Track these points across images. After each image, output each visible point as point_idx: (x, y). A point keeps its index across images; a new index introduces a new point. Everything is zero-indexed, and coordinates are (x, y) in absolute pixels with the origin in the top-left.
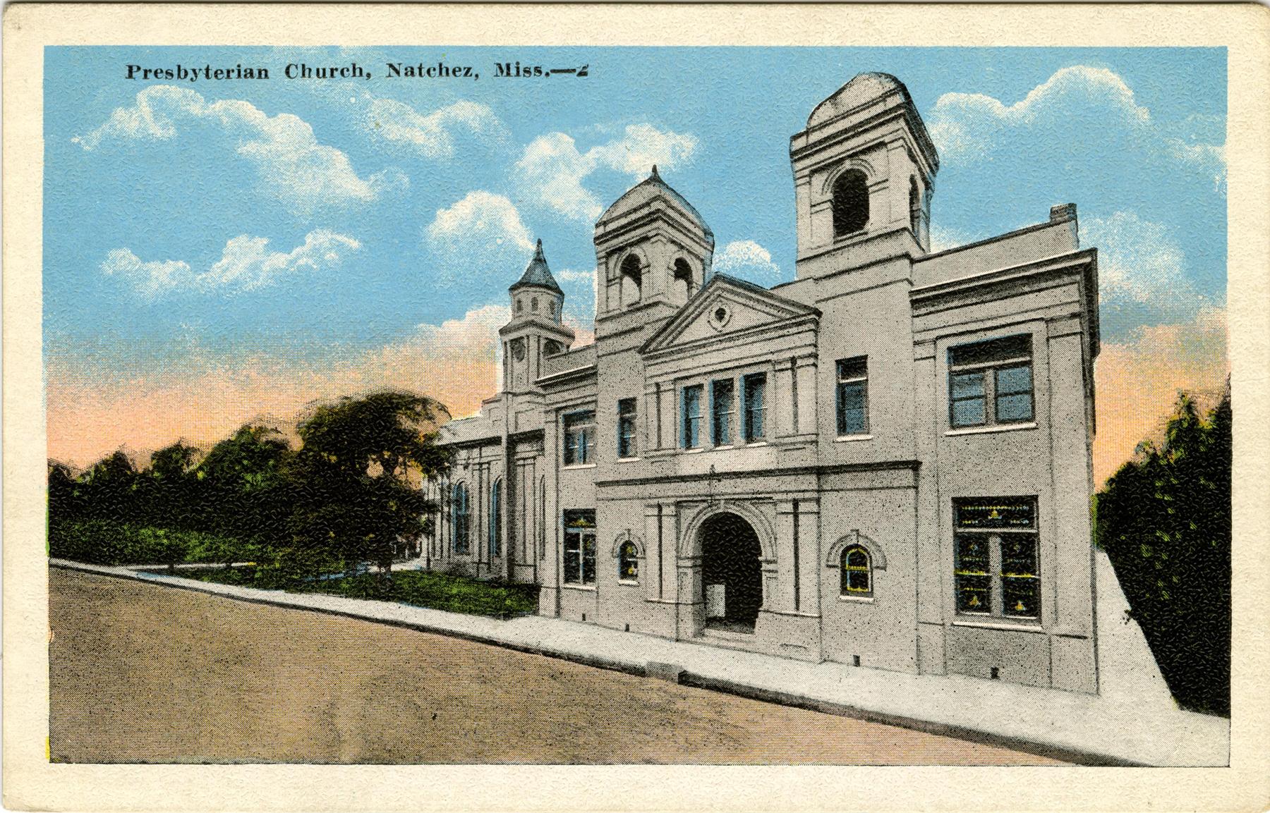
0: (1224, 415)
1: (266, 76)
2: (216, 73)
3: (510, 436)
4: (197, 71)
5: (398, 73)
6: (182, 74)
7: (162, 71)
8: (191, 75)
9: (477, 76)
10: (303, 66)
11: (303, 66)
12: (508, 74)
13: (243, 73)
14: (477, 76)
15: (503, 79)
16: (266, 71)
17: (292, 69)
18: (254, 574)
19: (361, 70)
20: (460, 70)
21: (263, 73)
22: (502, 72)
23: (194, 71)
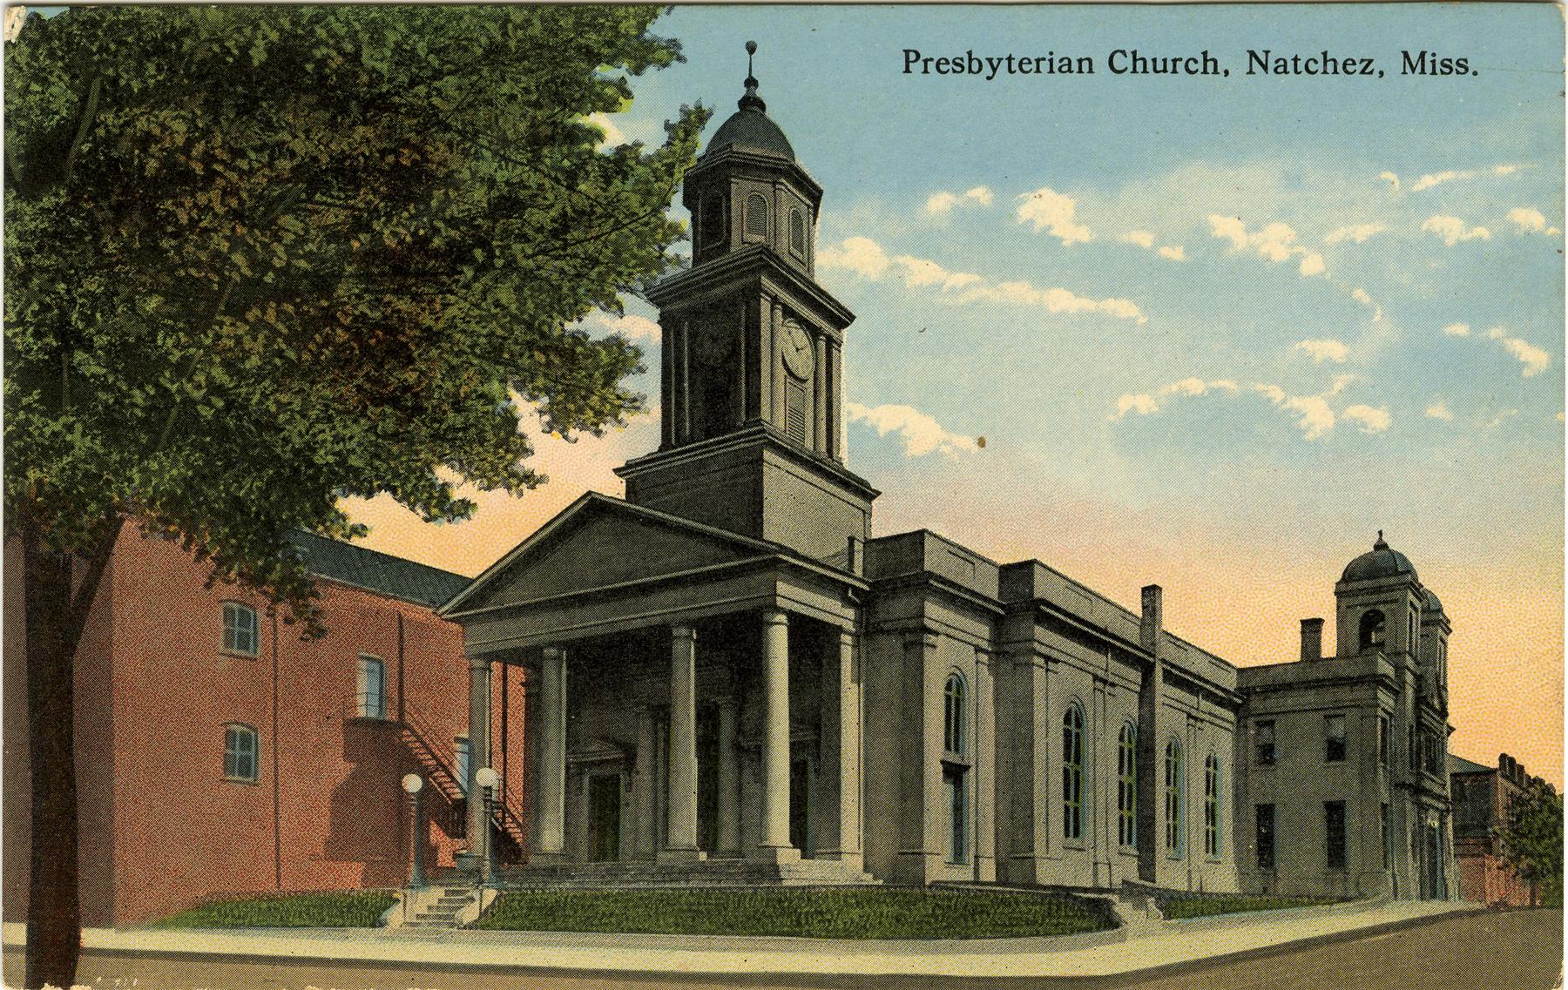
0: (711, 114)
1: (1091, 71)
2: (1345, 64)
3: (1033, 858)
4: (995, 63)
5: (1265, 68)
6: (975, 66)
7: (947, 62)
8: (987, 70)
9: (1381, 74)
10: (1134, 53)
11: (1134, 53)
12: (1423, 72)
13: (1056, 65)
14: (1381, 74)
15: (1414, 79)
16: (1089, 60)
17: (1118, 58)
18: (405, 279)
19: (1215, 62)
20: (1354, 63)
21: (1085, 65)
22: (1413, 70)
23: (990, 60)
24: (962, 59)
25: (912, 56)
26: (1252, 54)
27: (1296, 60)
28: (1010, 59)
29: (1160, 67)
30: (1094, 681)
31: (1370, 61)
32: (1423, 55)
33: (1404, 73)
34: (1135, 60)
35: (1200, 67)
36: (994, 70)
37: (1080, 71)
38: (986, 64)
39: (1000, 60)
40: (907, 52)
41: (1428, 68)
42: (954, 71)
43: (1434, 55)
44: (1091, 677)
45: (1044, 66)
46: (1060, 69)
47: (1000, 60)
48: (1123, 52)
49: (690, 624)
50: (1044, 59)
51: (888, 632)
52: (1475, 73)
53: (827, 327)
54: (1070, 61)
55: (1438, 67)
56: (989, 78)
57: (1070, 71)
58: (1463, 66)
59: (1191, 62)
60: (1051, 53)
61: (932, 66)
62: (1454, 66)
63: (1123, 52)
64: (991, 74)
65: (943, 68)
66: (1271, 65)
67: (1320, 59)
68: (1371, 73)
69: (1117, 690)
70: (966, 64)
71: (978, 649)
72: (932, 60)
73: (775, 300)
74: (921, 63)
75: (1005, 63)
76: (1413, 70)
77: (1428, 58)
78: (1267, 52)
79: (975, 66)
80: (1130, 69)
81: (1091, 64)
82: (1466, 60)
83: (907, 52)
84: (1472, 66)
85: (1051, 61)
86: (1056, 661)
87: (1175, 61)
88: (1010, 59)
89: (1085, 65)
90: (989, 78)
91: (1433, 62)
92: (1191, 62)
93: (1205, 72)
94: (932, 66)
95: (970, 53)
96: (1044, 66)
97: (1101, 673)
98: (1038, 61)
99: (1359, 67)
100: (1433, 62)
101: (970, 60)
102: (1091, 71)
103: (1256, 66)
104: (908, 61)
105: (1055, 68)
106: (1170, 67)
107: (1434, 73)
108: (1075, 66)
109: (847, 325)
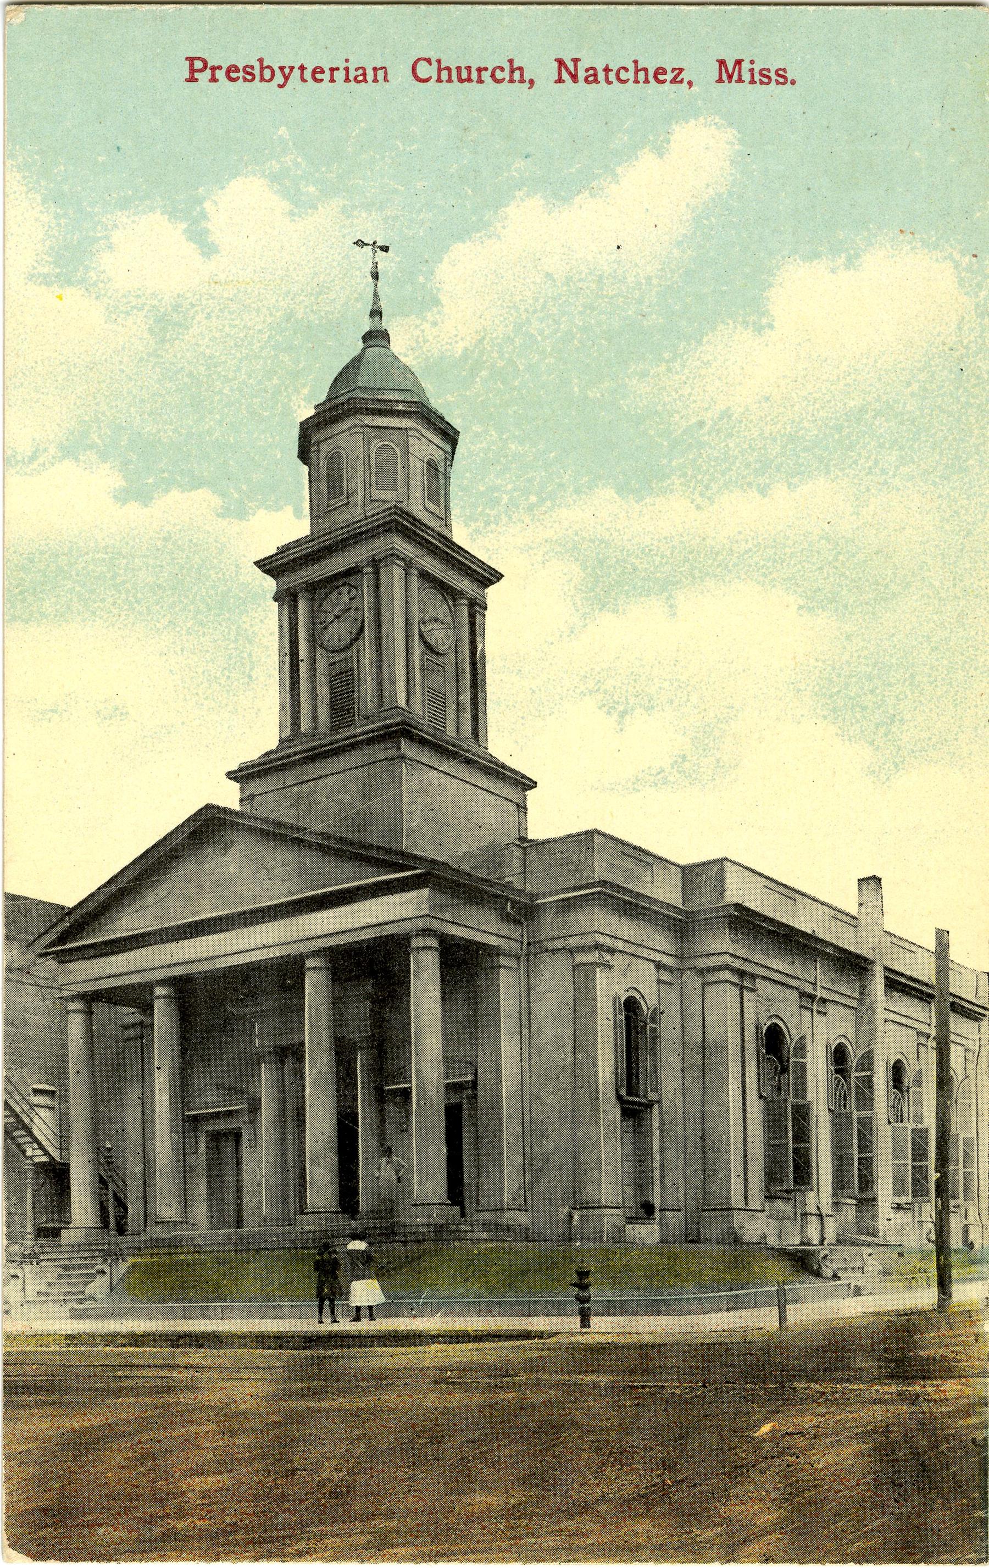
1: (386, 79)
2: (314, 72)
5: (574, 78)
6: (267, 74)
7: (237, 70)
8: (279, 79)
10: (439, 61)
11: (439, 61)
13: (352, 75)
14: (690, 84)
21: (380, 74)
23: (282, 68)
24: (252, 67)
25: (198, 64)
26: (561, 63)
27: (607, 70)
28: (302, 68)
29: (464, 75)
30: (800, 997)
31: (681, 70)
32: (739, 62)
33: (560, 80)
34: (440, 70)
35: (506, 75)
36: (286, 78)
37: (375, 80)
38: (278, 73)
39: (292, 68)
40: (191, 60)
41: (746, 76)
42: (245, 80)
43: (752, 62)
44: (796, 994)
45: (339, 75)
46: (355, 79)
47: (292, 68)
48: (429, 61)
49: (316, 954)
50: (338, 69)
51: (555, 951)
52: (690, 84)
53: (465, 585)
54: (364, 69)
55: (757, 77)
56: (280, 86)
57: (365, 80)
58: (782, 77)
59: (622, 71)
60: (347, 61)
61: (220, 74)
62: (774, 77)
63: (429, 61)
64: (281, 81)
65: (233, 75)
66: (582, 74)
67: (507, 66)
68: (681, 82)
69: (831, 1008)
70: (257, 72)
71: (659, 966)
72: (486, 69)
73: (408, 565)
74: (208, 73)
75: (297, 72)
76: (730, 77)
77: (746, 66)
78: (576, 61)
79: (267, 74)
80: (435, 77)
81: (386, 73)
82: (784, 70)
83: (191, 60)
84: (790, 76)
85: (347, 69)
86: (753, 976)
87: (479, 70)
88: (302, 68)
89: (380, 74)
90: (280, 86)
91: (752, 70)
92: (622, 71)
93: (636, 81)
94: (220, 74)
95: (261, 60)
96: (339, 75)
97: (809, 989)
98: (332, 70)
99: (669, 76)
100: (752, 70)
101: (262, 69)
102: (386, 79)
103: (565, 76)
104: (192, 70)
105: (351, 77)
106: (474, 75)
107: (753, 81)
108: (370, 77)
109: (492, 583)
